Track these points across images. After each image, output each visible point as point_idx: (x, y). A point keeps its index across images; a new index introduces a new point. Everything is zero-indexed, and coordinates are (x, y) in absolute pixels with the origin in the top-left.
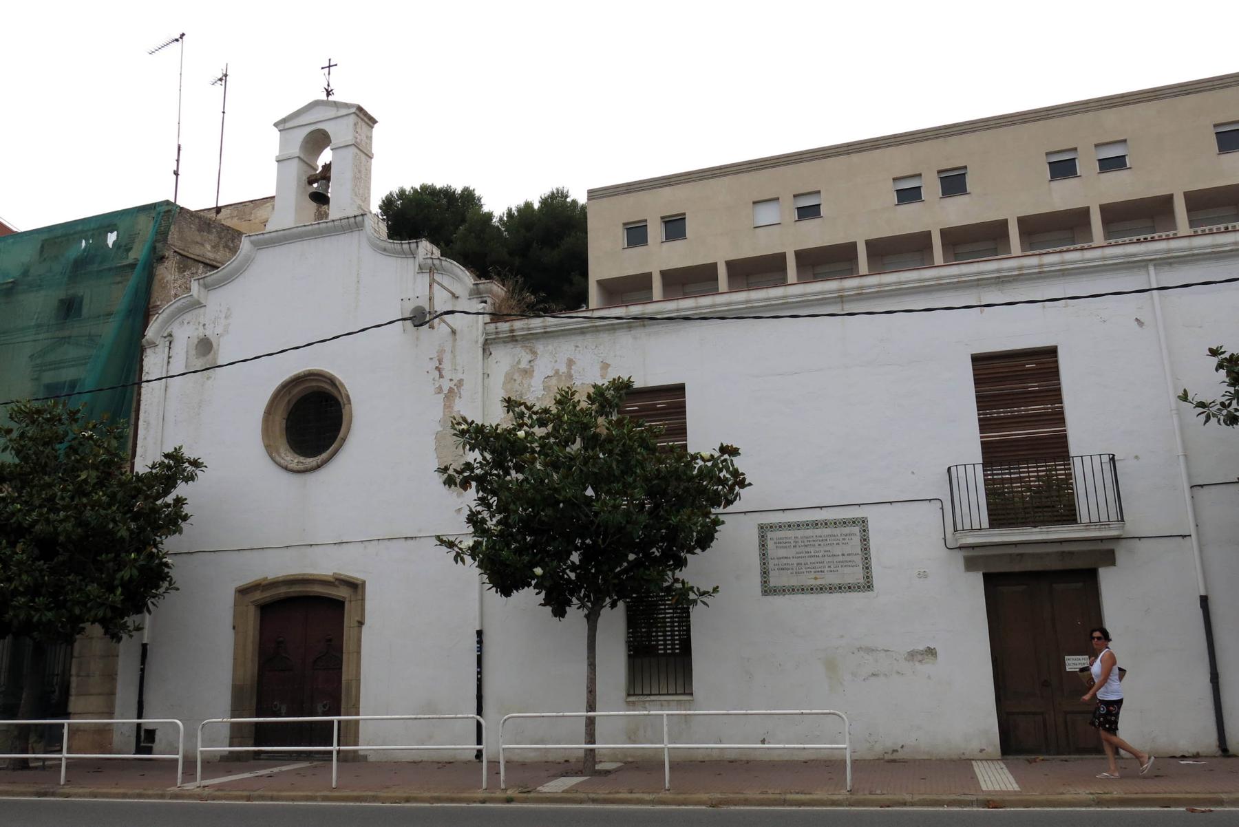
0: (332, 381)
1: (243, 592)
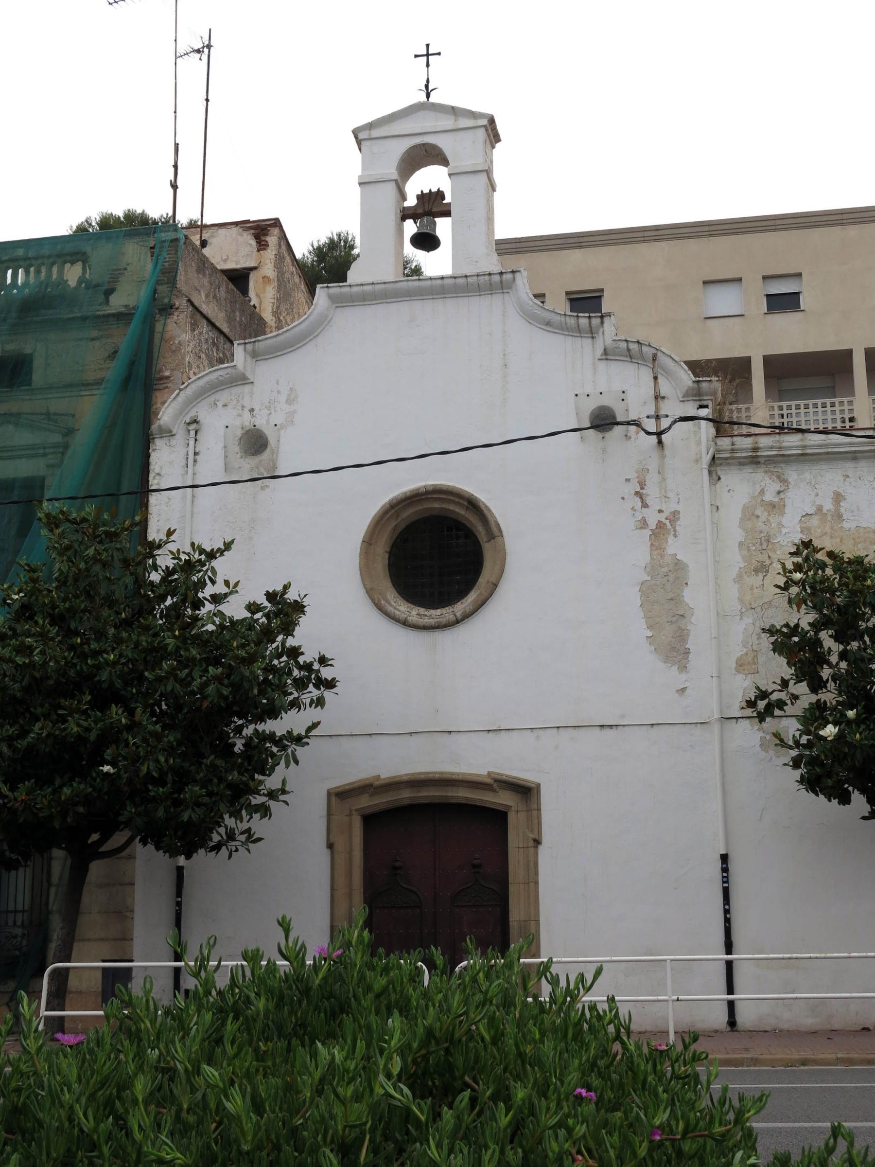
0: (473, 504)
1: (340, 796)
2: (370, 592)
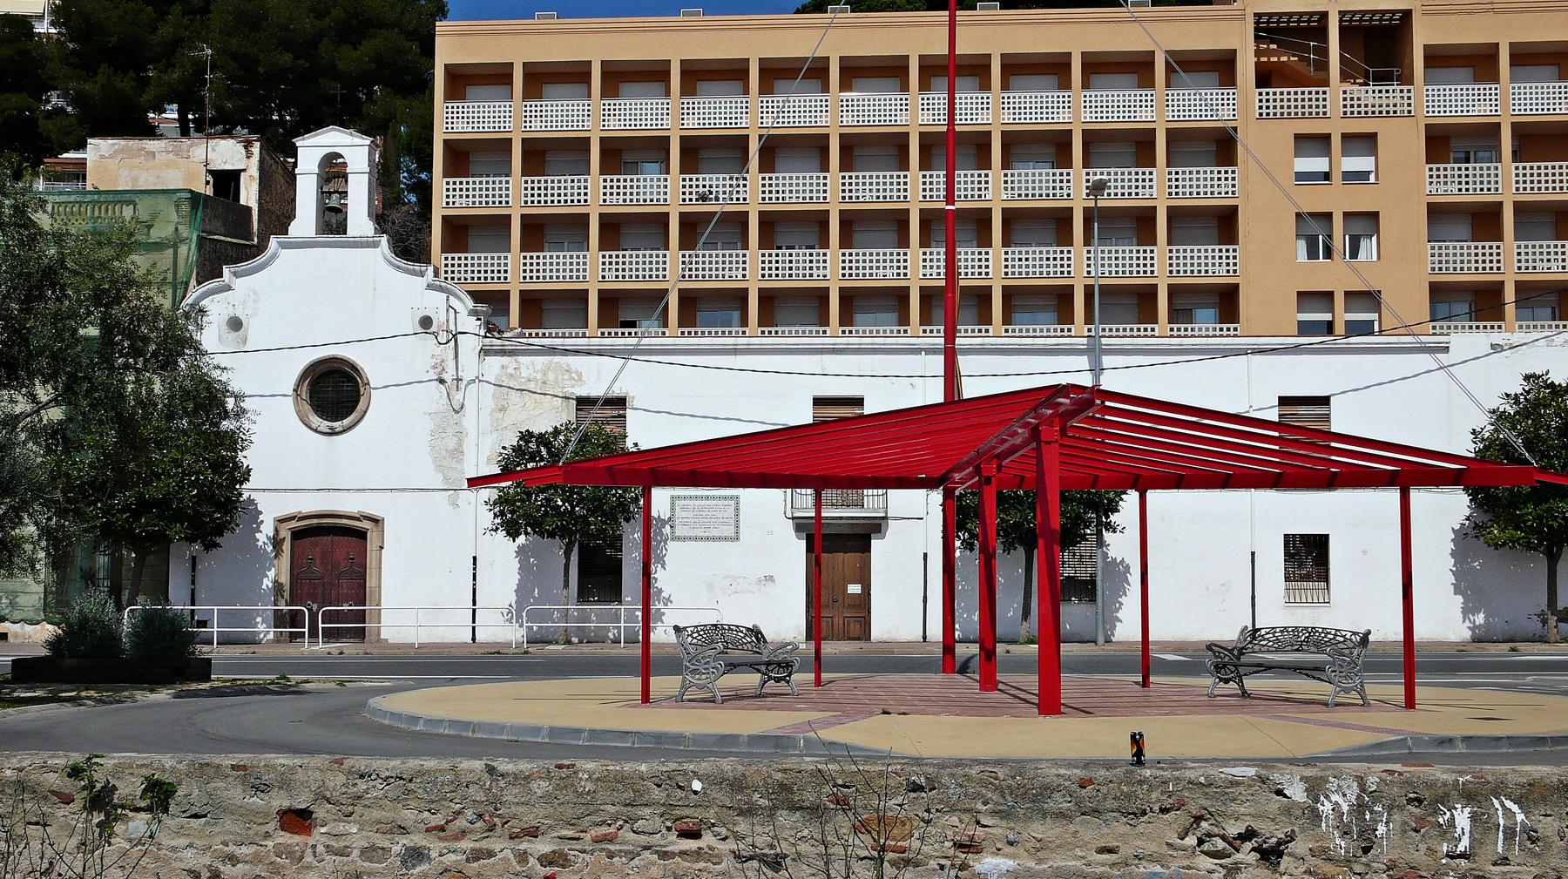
0: (354, 367)
2: (298, 412)
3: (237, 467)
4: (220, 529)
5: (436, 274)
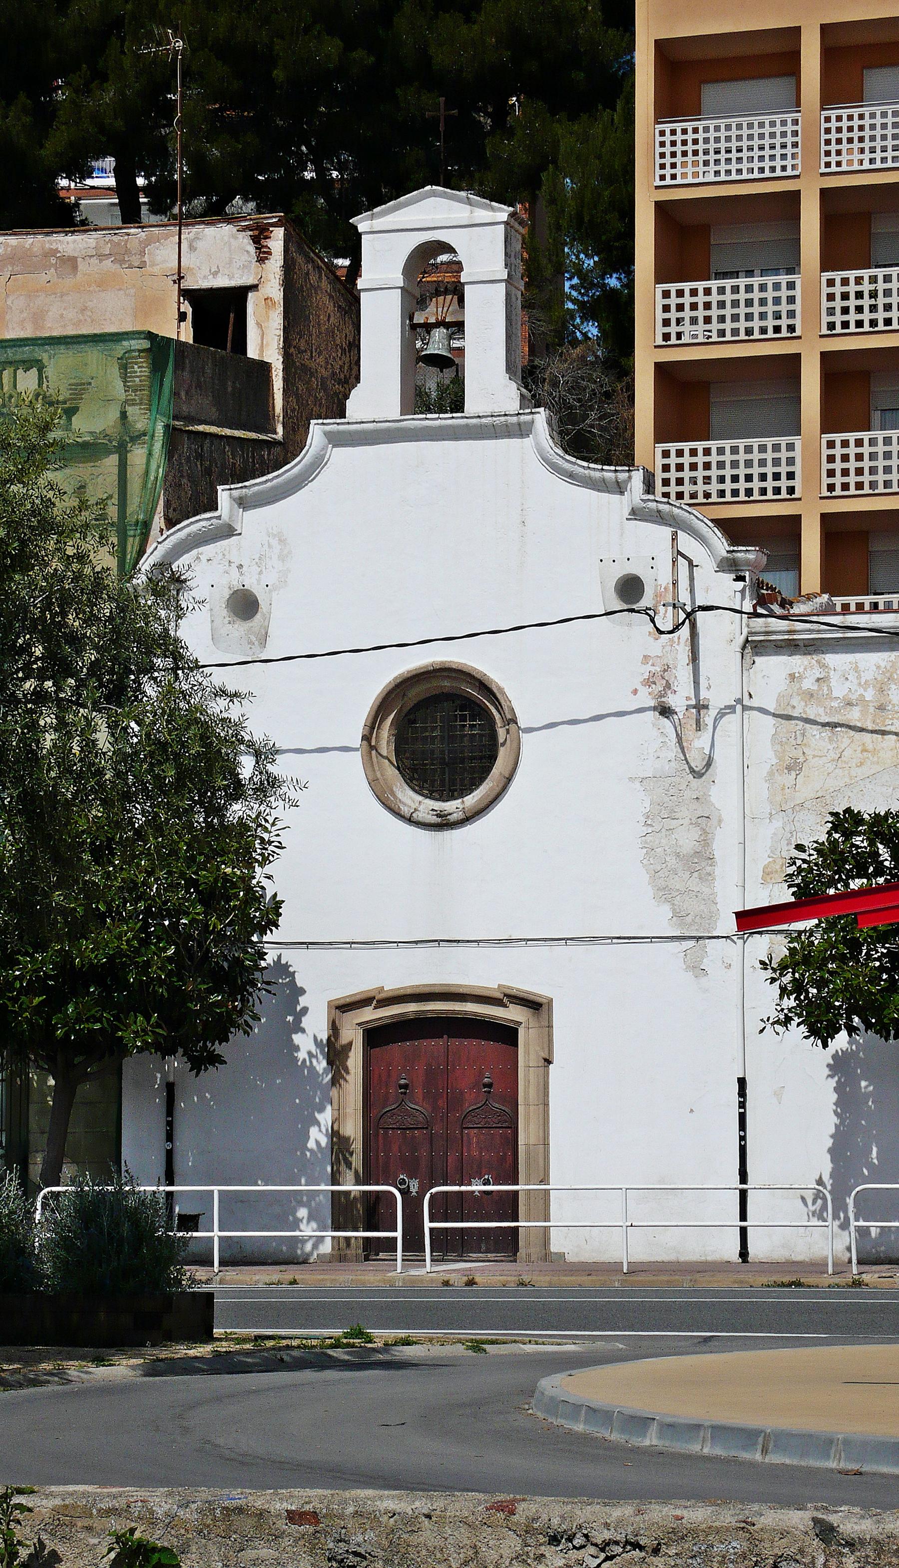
0: (484, 686)
3: (253, 897)
4: (221, 1028)
5: (649, 487)
